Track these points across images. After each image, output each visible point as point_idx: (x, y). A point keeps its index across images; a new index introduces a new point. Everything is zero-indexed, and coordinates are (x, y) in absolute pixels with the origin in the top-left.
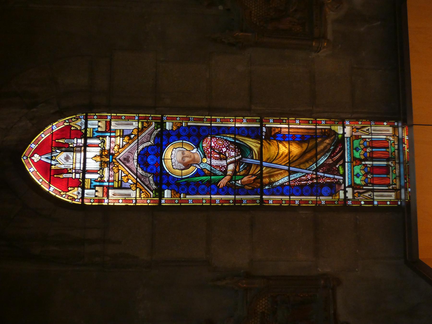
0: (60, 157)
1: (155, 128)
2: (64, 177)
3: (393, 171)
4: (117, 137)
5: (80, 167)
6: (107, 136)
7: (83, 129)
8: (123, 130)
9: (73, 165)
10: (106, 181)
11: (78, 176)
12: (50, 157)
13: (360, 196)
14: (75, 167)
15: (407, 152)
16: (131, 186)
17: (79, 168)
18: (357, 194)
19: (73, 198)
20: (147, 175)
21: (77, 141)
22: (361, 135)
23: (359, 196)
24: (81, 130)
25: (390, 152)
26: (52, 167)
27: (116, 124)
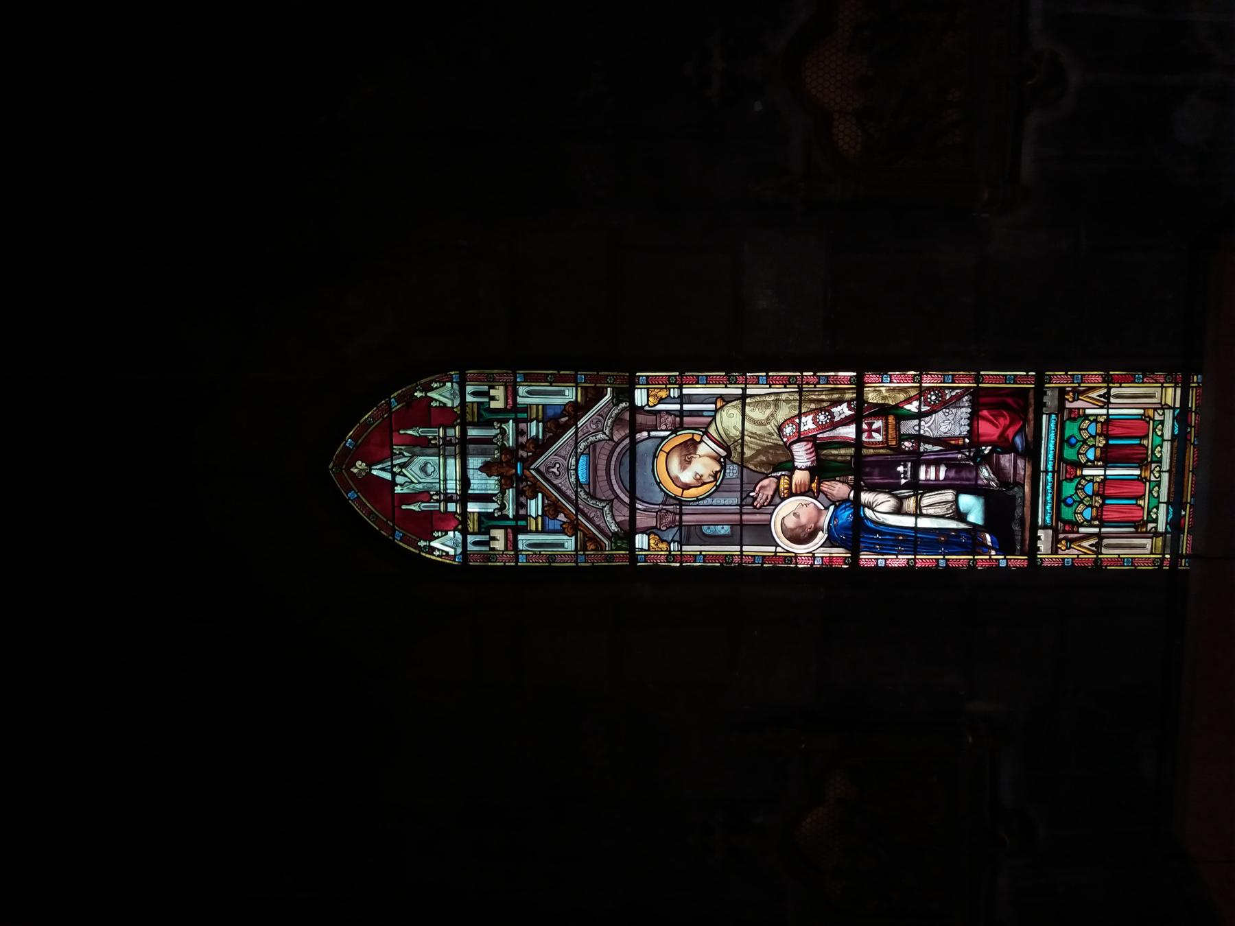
0: (411, 467)
1: (613, 402)
2: (423, 509)
3: (1151, 511)
4: (531, 421)
5: (456, 489)
6: (510, 419)
7: (457, 406)
8: (544, 406)
9: (440, 483)
10: (511, 516)
11: (452, 507)
12: (390, 467)
13: (1070, 548)
14: (446, 489)
15: (1185, 510)
16: (564, 526)
17: (454, 491)
18: (1063, 542)
19: (444, 554)
20: (595, 504)
21: (445, 432)
22: (1084, 409)
23: (1067, 549)
24: (453, 408)
25: (1150, 447)
26: (396, 488)
27: (527, 392)
